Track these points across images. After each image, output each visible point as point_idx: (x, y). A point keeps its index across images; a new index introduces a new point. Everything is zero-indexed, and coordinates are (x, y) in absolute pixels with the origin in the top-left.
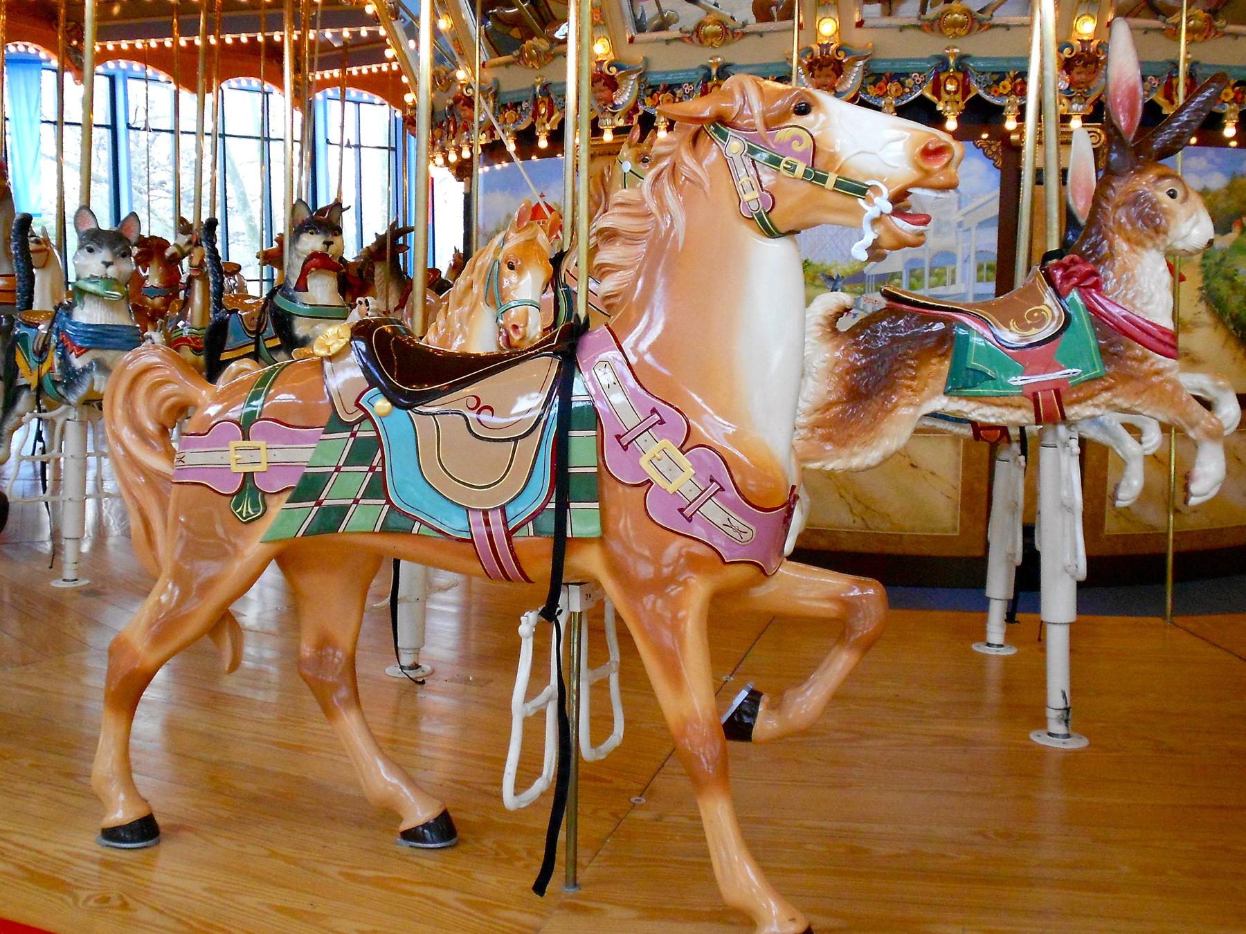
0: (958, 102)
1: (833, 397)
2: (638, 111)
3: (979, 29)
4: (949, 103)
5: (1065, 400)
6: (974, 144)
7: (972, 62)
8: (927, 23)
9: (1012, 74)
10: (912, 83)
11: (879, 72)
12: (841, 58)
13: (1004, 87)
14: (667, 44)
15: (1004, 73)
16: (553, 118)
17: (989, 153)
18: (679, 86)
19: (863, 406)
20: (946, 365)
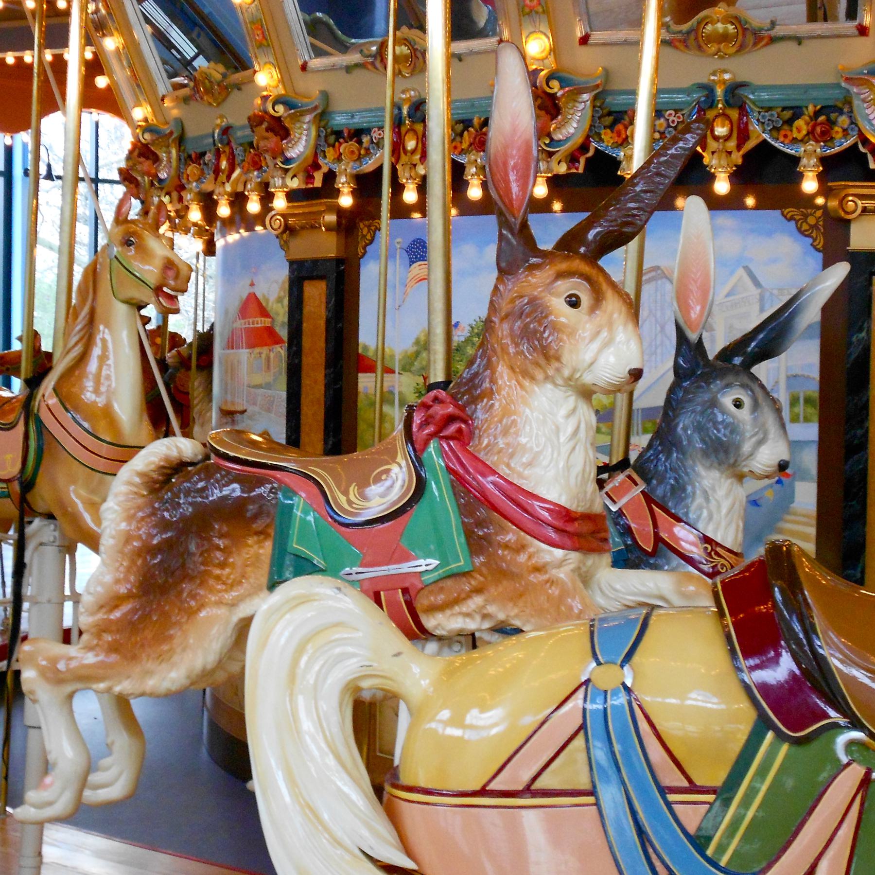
0: (730, 153)
1: (123, 590)
2: (588, 150)
4: (716, 155)
5: (421, 603)
6: (783, 214)
7: (753, 93)
8: (679, 36)
9: (811, 109)
10: (665, 125)
11: (617, 109)
12: (555, 90)
13: (799, 131)
14: (347, 72)
15: (800, 108)
19: (159, 604)
20: (266, 549)
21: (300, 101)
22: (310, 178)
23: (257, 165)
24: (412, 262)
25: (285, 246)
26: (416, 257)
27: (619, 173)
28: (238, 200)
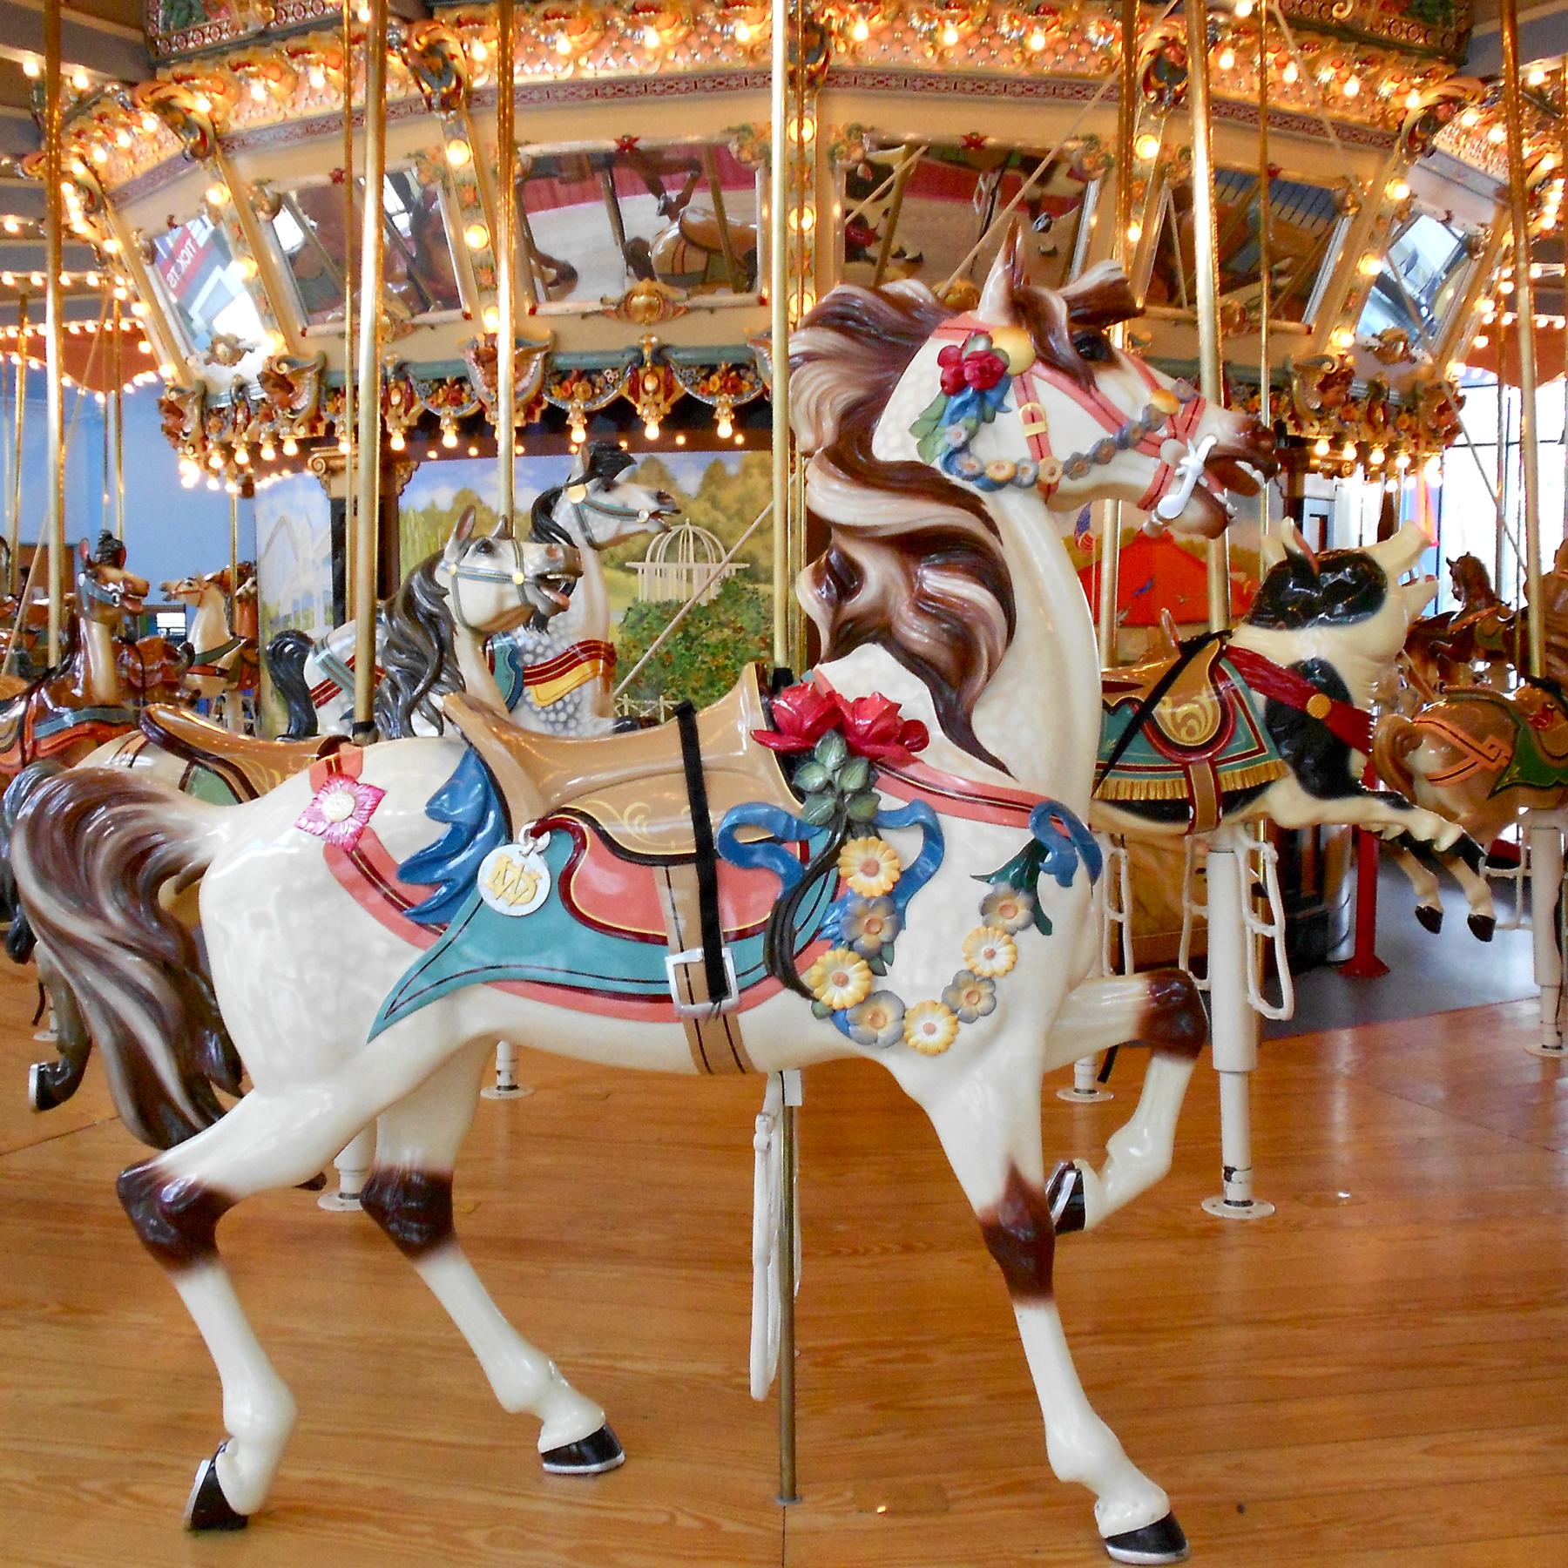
3: (674, 314)
16: (413, 411)
18: (599, 372)
21: (299, 360)
22: (313, 429)
23: (269, 417)
25: (326, 486)
28: (254, 449)
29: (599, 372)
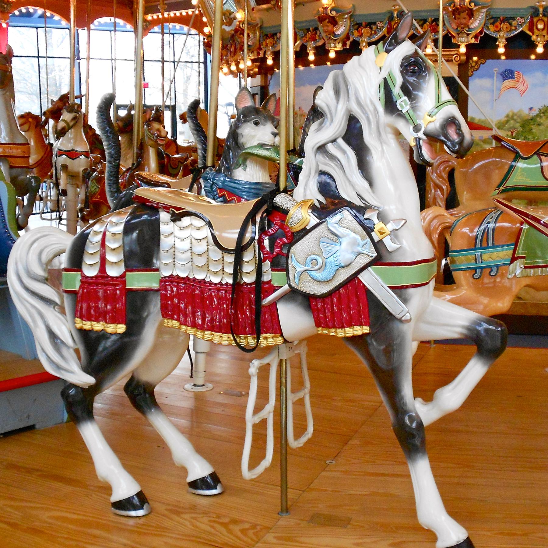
0: (544, 36)
10: (516, 23)
17: (476, 67)
24: (504, 80)
26: (507, 77)
27: (497, 43)
29: (375, 23)
